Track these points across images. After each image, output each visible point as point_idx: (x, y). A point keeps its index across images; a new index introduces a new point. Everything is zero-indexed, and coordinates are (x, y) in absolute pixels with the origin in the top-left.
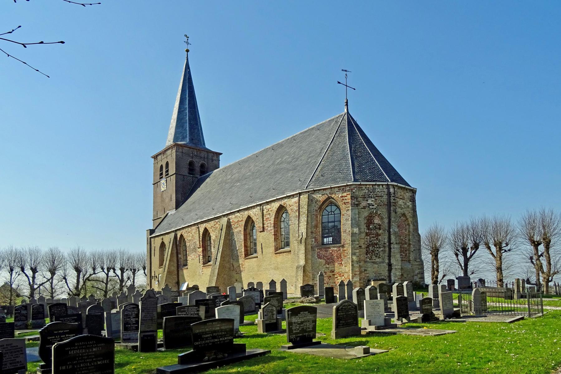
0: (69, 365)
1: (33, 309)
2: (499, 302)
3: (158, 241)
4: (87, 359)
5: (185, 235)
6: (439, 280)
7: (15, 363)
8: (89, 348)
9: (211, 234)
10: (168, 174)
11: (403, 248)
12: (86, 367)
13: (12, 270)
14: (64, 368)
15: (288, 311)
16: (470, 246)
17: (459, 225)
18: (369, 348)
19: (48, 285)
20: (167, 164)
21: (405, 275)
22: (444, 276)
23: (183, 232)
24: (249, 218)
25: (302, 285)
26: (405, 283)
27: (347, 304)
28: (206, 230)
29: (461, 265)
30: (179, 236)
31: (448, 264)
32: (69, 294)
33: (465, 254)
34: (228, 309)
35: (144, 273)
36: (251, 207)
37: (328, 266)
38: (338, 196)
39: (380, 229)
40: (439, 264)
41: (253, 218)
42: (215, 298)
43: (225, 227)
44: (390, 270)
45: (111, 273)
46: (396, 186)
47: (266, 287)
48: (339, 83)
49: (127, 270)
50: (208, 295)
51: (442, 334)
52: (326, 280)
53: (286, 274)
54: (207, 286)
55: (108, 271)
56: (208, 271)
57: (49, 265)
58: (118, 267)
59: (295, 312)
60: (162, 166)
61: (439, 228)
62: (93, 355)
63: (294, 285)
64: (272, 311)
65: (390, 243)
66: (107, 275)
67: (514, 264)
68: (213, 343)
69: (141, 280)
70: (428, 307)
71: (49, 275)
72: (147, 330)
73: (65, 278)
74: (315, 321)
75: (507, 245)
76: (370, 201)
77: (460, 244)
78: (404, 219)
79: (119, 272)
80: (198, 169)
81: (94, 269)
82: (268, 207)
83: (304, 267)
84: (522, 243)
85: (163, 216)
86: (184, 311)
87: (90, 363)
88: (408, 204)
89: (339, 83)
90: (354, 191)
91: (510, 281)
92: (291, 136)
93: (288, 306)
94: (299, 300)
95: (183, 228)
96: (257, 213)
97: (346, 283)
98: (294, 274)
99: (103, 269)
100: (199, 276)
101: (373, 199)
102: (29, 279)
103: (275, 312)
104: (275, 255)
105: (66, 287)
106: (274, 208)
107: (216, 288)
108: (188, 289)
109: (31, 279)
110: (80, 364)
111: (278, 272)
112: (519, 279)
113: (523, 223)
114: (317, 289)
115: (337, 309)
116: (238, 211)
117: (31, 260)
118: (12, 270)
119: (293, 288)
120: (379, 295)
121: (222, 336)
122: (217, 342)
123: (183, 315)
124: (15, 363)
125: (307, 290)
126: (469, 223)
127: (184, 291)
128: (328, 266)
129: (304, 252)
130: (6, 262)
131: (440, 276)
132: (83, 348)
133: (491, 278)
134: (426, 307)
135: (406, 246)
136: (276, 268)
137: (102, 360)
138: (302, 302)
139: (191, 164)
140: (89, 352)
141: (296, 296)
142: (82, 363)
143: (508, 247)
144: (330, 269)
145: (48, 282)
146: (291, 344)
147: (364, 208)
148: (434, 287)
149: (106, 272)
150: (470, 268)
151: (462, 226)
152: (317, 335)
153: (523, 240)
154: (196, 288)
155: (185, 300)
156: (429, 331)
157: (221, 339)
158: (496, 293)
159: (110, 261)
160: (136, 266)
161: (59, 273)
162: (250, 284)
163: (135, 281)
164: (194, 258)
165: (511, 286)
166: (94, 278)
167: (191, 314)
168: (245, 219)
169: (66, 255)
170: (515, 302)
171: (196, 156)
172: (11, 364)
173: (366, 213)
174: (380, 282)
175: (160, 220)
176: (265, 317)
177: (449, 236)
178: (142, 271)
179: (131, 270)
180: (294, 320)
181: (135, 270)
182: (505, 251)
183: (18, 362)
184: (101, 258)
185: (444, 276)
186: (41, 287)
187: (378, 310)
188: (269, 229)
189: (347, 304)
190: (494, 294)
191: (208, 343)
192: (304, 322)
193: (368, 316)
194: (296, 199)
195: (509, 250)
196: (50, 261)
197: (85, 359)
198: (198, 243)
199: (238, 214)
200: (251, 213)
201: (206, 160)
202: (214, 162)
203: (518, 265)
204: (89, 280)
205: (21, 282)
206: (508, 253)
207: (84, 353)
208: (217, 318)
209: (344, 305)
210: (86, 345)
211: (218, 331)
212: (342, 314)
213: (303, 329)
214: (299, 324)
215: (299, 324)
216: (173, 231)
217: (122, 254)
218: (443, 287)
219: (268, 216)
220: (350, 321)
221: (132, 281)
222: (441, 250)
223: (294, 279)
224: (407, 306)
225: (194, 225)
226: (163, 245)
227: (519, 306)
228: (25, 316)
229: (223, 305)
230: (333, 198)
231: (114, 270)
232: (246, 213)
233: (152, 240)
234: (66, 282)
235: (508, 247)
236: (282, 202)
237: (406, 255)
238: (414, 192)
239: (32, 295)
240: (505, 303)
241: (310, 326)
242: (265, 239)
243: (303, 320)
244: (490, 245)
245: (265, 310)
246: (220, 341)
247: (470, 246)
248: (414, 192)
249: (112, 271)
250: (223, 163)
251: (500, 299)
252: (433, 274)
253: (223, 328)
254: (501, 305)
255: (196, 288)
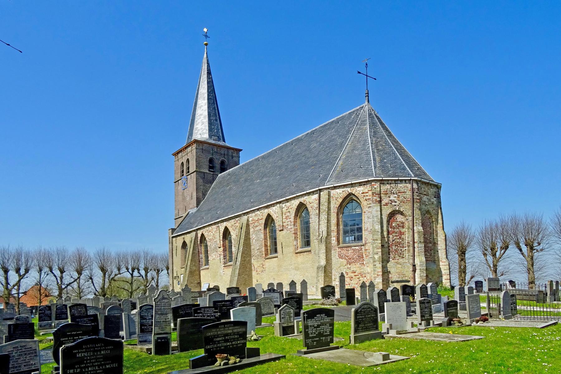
0: (77, 368)
1: (57, 309)
2: (530, 306)
3: (180, 241)
4: (95, 362)
5: (206, 234)
6: (466, 282)
7: (29, 365)
8: (97, 351)
9: (232, 233)
10: (188, 172)
11: (428, 247)
12: (94, 370)
13: (41, 270)
14: (72, 371)
15: (304, 313)
16: (499, 245)
17: (488, 223)
18: (388, 355)
19: (75, 285)
20: (188, 160)
21: (430, 276)
22: (472, 277)
23: (204, 231)
24: (269, 216)
25: (323, 286)
26: (429, 284)
27: (366, 306)
28: (226, 229)
29: (490, 266)
30: (199, 235)
31: (477, 264)
32: (95, 294)
33: (494, 255)
34: (243, 311)
35: (168, 273)
36: (271, 205)
37: (349, 266)
38: (358, 191)
39: (403, 227)
40: (467, 265)
41: (273, 217)
42: (234, 299)
43: (245, 225)
44: (414, 271)
45: (136, 273)
46: (420, 181)
47: (286, 288)
48: (359, 73)
49: (151, 270)
50: (227, 296)
51: (468, 340)
52: (347, 280)
53: (307, 274)
54: (228, 287)
55: (133, 271)
56: (229, 271)
57: (75, 265)
58: (142, 266)
59: (312, 314)
60: (182, 163)
61: (466, 227)
62: (101, 358)
63: (315, 287)
64: (289, 313)
65: (414, 243)
66: (132, 275)
67: (547, 264)
68: (226, 347)
69: (164, 279)
70: (454, 311)
71: (76, 275)
72: (161, 332)
73: (91, 278)
74: (332, 325)
75: (539, 244)
76: (392, 198)
77: (488, 243)
78: (429, 216)
79: (143, 272)
80: (218, 166)
81: (119, 269)
82: (288, 204)
83: (325, 267)
84: (556, 242)
85: (184, 215)
86: (201, 313)
87: (99, 366)
88: (432, 200)
89: (359, 73)
90: (375, 186)
91: (542, 284)
92: (310, 131)
93: (306, 307)
94: (320, 302)
95: (204, 227)
96: (276, 210)
97: (367, 284)
98: (314, 274)
99: (127, 269)
100: (218, 276)
101: (396, 195)
102: (57, 279)
103: (292, 315)
104: (295, 255)
105: (93, 287)
106: (294, 205)
107: (237, 290)
108: (209, 289)
109: (59, 279)
110: (88, 367)
111: (298, 272)
112: (552, 281)
113: (557, 220)
114: (337, 290)
115: (356, 312)
116: (258, 209)
117: (59, 260)
118: (41, 270)
119: (314, 289)
120: (401, 297)
121: (234, 340)
122: (229, 345)
123: (199, 316)
124: (29, 365)
125: (327, 292)
126: (498, 221)
127: (205, 292)
128: (349, 266)
129: (324, 251)
130: (35, 261)
131: (468, 277)
132: (91, 351)
133: (522, 279)
134: (452, 311)
135: (430, 245)
136: (297, 269)
137: (111, 364)
138: (323, 304)
139: (211, 161)
140: (97, 355)
141: (317, 298)
142: (91, 366)
143: (541, 247)
144: (352, 269)
145: (75, 283)
146: (305, 349)
147: (386, 204)
148: (460, 288)
149: (131, 273)
150: (500, 269)
151: (491, 225)
152: (335, 339)
153: (556, 239)
154: (216, 288)
155: (204, 302)
156: (454, 337)
157: (233, 343)
158: (529, 297)
159: (134, 261)
160: (160, 266)
161: (86, 273)
162: (271, 285)
163: (159, 281)
164: (216, 256)
165: (544, 288)
166: (120, 278)
167: (208, 316)
168: (265, 217)
169: (92, 255)
170: (548, 306)
171: (217, 152)
172: (25, 366)
173: (387, 211)
174: (404, 284)
175: (181, 219)
176: (283, 320)
177: (477, 234)
178: (165, 272)
179: (155, 270)
180: (310, 322)
181: (158, 271)
182: (537, 251)
183: (32, 364)
184: (125, 257)
185: (472, 277)
186: (69, 287)
187: (400, 313)
188: (289, 227)
189: (366, 306)
190: (525, 297)
191: (220, 347)
192: (320, 325)
193: (389, 320)
194: (316, 196)
195: (542, 250)
196: (76, 260)
197: (93, 363)
198: (218, 242)
199: (258, 212)
200: (306, 200)
201: (226, 156)
202: (234, 159)
203: (550, 266)
204: (115, 280)
205: (50, 281)
206: (541, 253)
207: (92, 356)
208: (232, 320)
209: (363, 307)
210: (94, 348)
211: (230, 334)
212: (361, 317)
213: (320, 333)
214: (315, 327)
215: (315, 327)
216: (194, 231)
217: (146, 254)
218: (471, 289)
219: (288, 214)
220: (370, 324)
221: (156, 281)
222: (469, 249)
223: (315, 279)
224: (431, 309)
225: (215, 224)
226: (184, 245)
227: (552, 310)
228: (49, 317)
229: (240, 306)
230: (354, 195)
231: (139, 270)
232: (266, 211)
233: (174, 239)
234: (92, 282)
235: (541, 247)
236: (301, 200)
237: (431, 255)
238: (438, 187)
239: (60, 295)
240: (537, 306)
241: (327, 329)
242: (287, 237)
243: (319, 323)
244: (521, 244)
245: (282, 313)
246: (232, 345)
247: (499, 245)
248: (438, 187)
249: (136, 271)
250: (244, 160)
251: (532, 302)
252: (461, 276)
253: (235, 331)
254: (532, 309)
255: (216, 288)
